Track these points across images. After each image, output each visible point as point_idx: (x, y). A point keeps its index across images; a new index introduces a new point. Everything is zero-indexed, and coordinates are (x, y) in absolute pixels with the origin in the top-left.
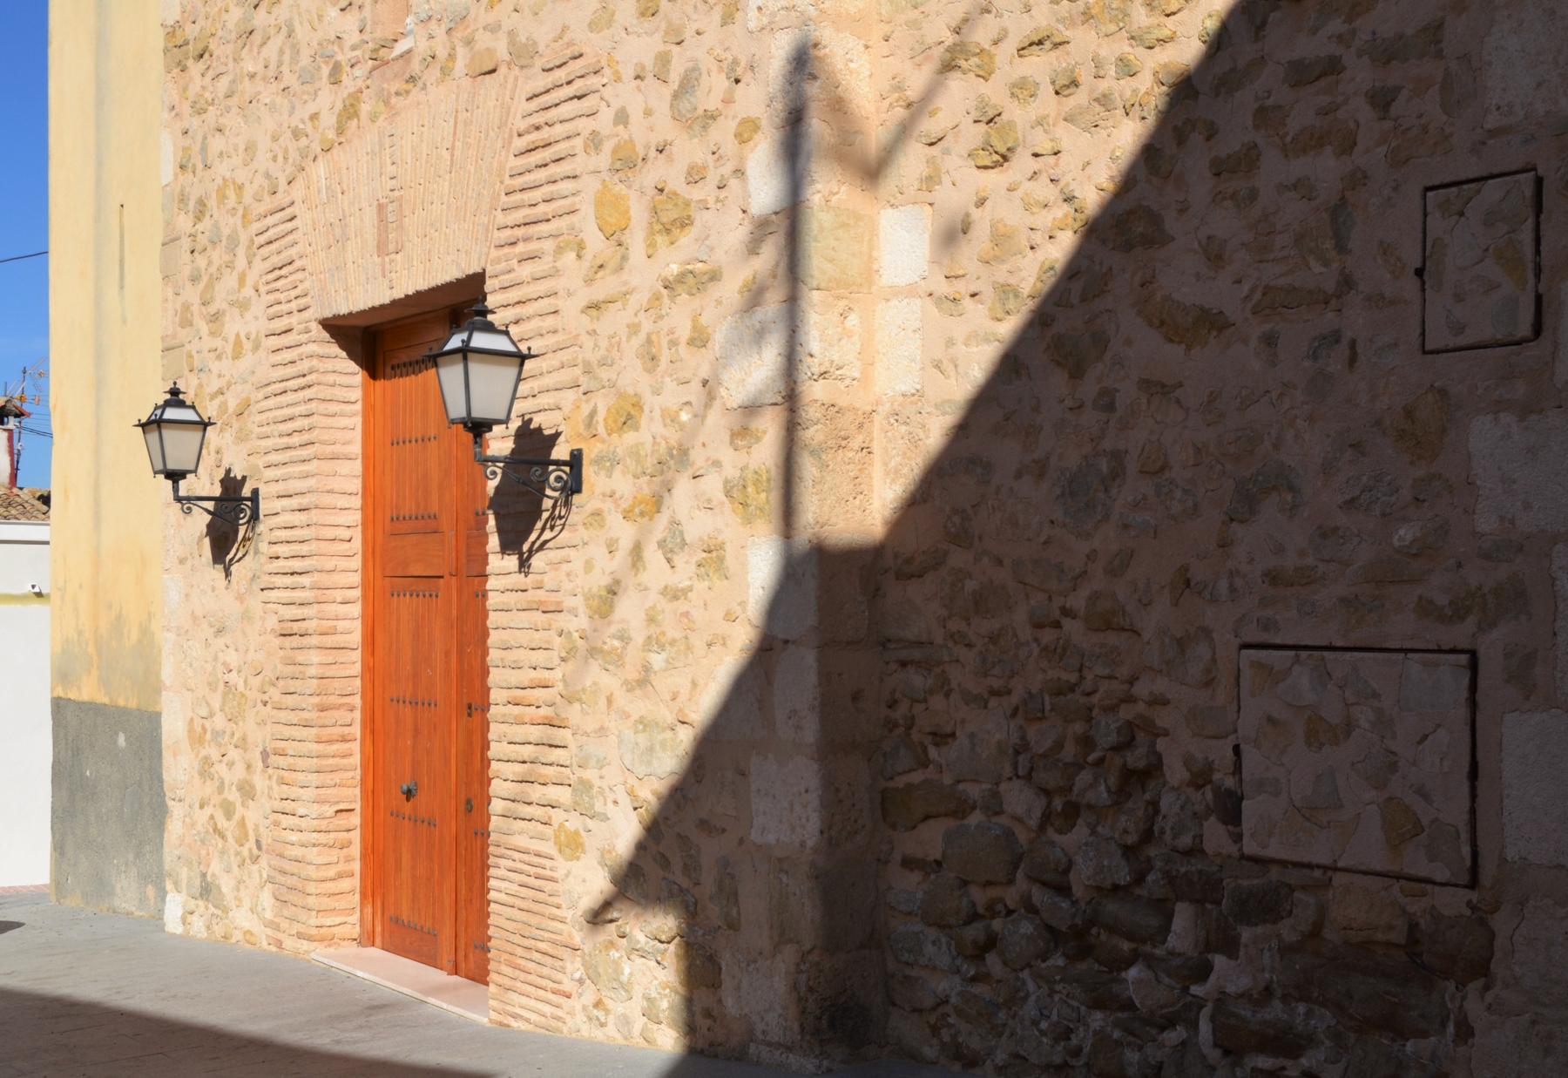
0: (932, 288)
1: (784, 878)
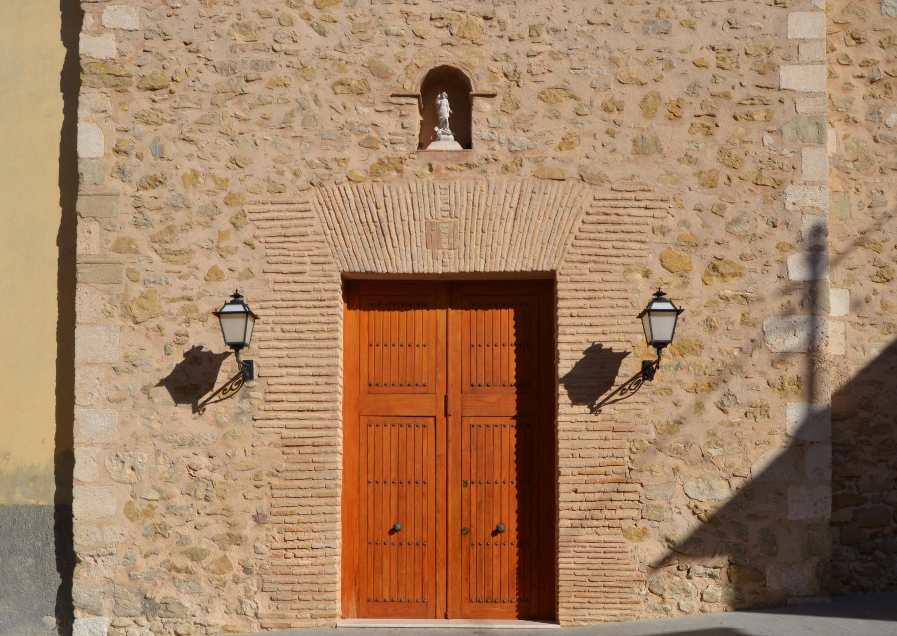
0: (851, 319)
1: (811, 532)
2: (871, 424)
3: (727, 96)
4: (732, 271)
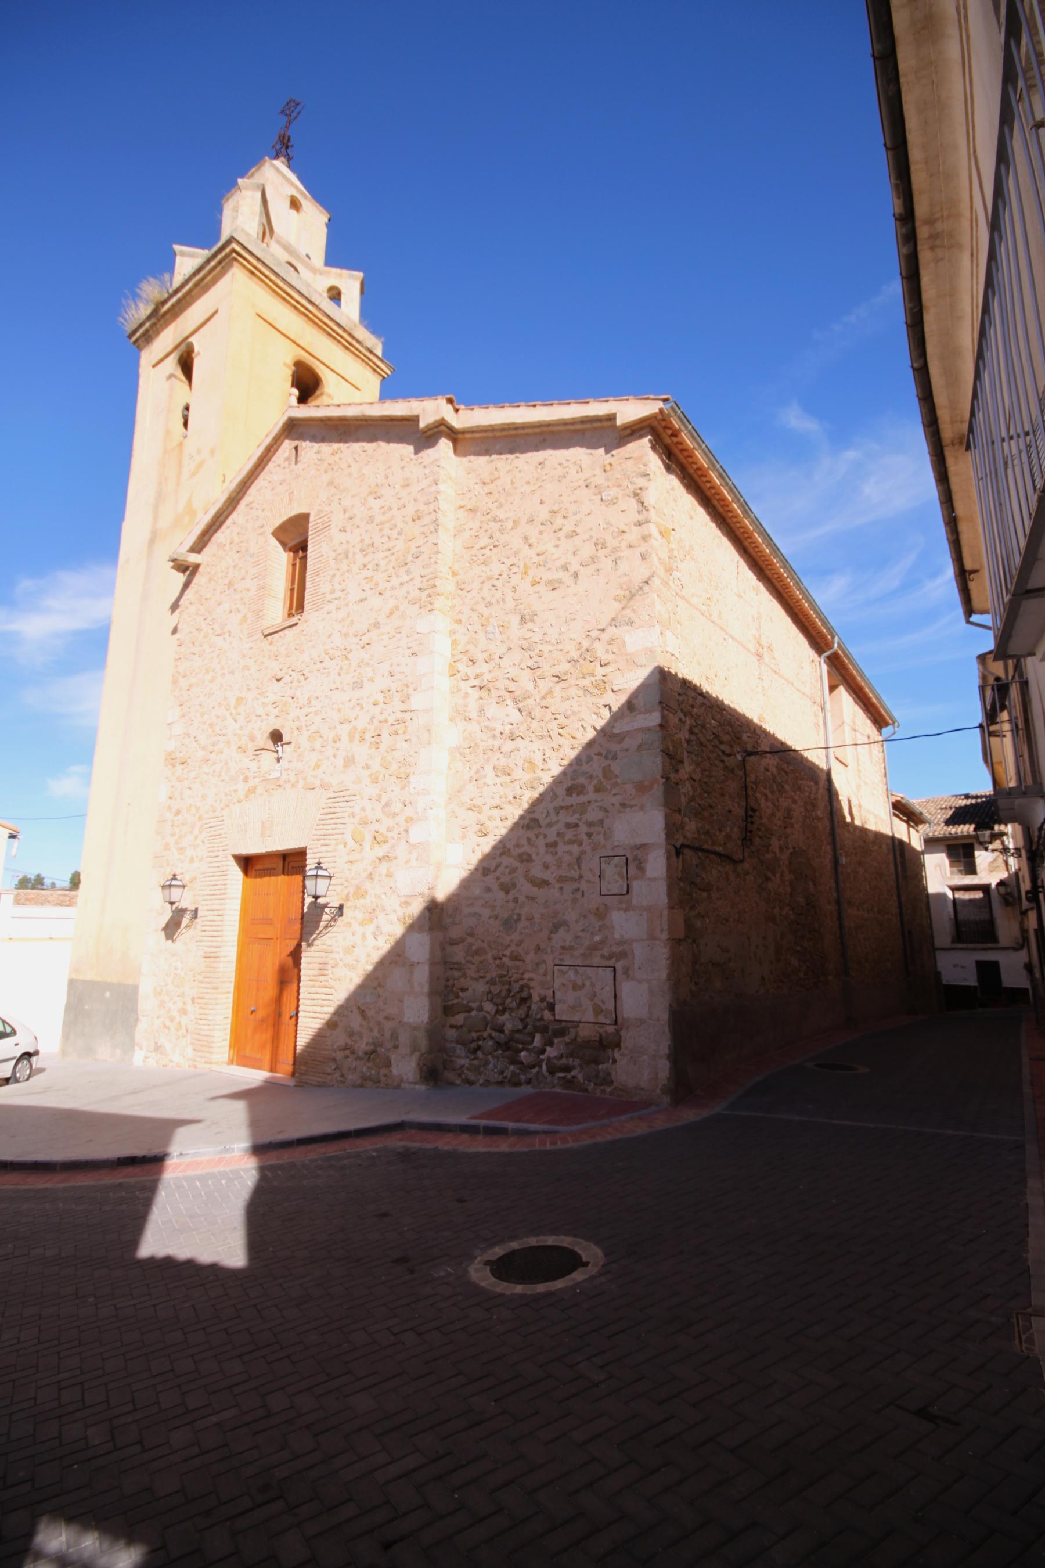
2: (474, 948)
3: (386, 721)
4: (383, 839)
